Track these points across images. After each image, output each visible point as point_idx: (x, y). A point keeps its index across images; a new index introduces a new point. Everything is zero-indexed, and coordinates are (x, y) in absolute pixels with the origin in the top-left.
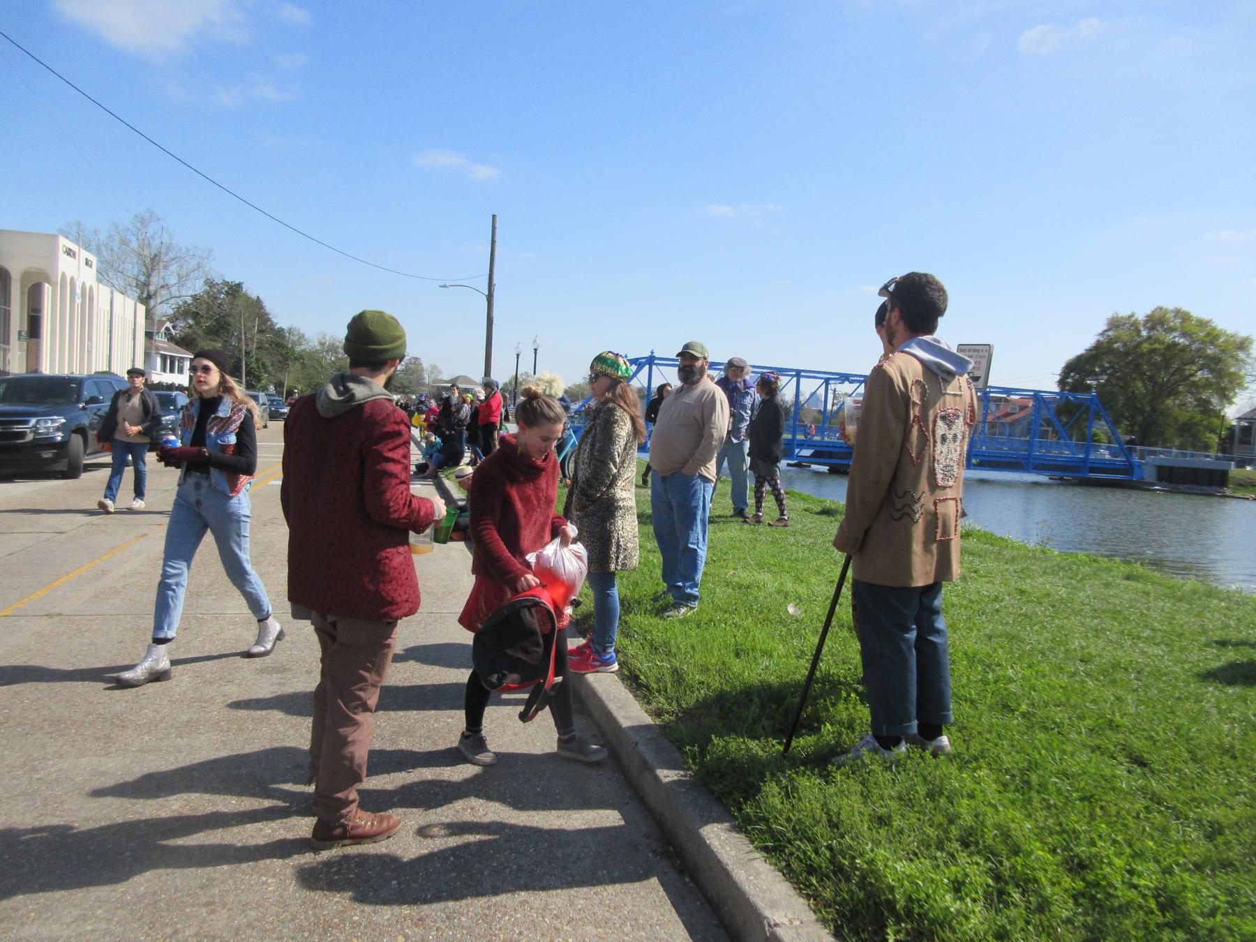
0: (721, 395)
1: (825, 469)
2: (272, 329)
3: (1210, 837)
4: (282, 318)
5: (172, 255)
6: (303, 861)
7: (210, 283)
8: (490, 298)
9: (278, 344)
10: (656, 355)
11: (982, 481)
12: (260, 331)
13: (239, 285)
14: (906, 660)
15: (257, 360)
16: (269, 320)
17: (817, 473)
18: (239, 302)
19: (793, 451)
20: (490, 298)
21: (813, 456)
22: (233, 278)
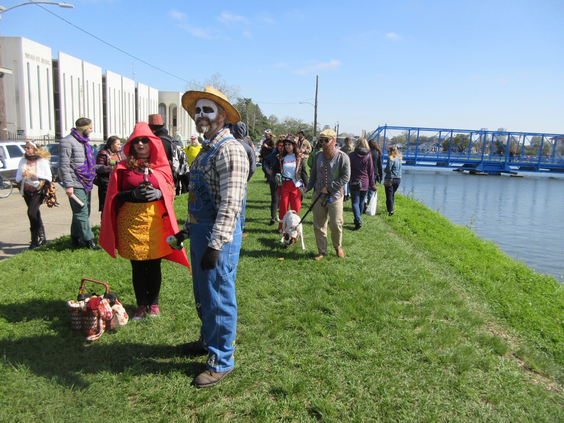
0: (36, 142)
1: (468, 172)
2: (262, 116)
3: (364, 290)
4: (266, 112)
5: (225, 90)
6: (162, 361)
7: (240, 100)
8: (316, 107)
9: (264, 123)
10: (388, 125)
11: (551, 178)
12: (256, 118)
13: (250, 100)
14: (339, 235)
15: (255, 130)
16: (261, 113)
17: (466, 174)
18: (249, 107)
19: (448, 164)
20: (316, 107)
21: (463, 166)
22: (248, 97)
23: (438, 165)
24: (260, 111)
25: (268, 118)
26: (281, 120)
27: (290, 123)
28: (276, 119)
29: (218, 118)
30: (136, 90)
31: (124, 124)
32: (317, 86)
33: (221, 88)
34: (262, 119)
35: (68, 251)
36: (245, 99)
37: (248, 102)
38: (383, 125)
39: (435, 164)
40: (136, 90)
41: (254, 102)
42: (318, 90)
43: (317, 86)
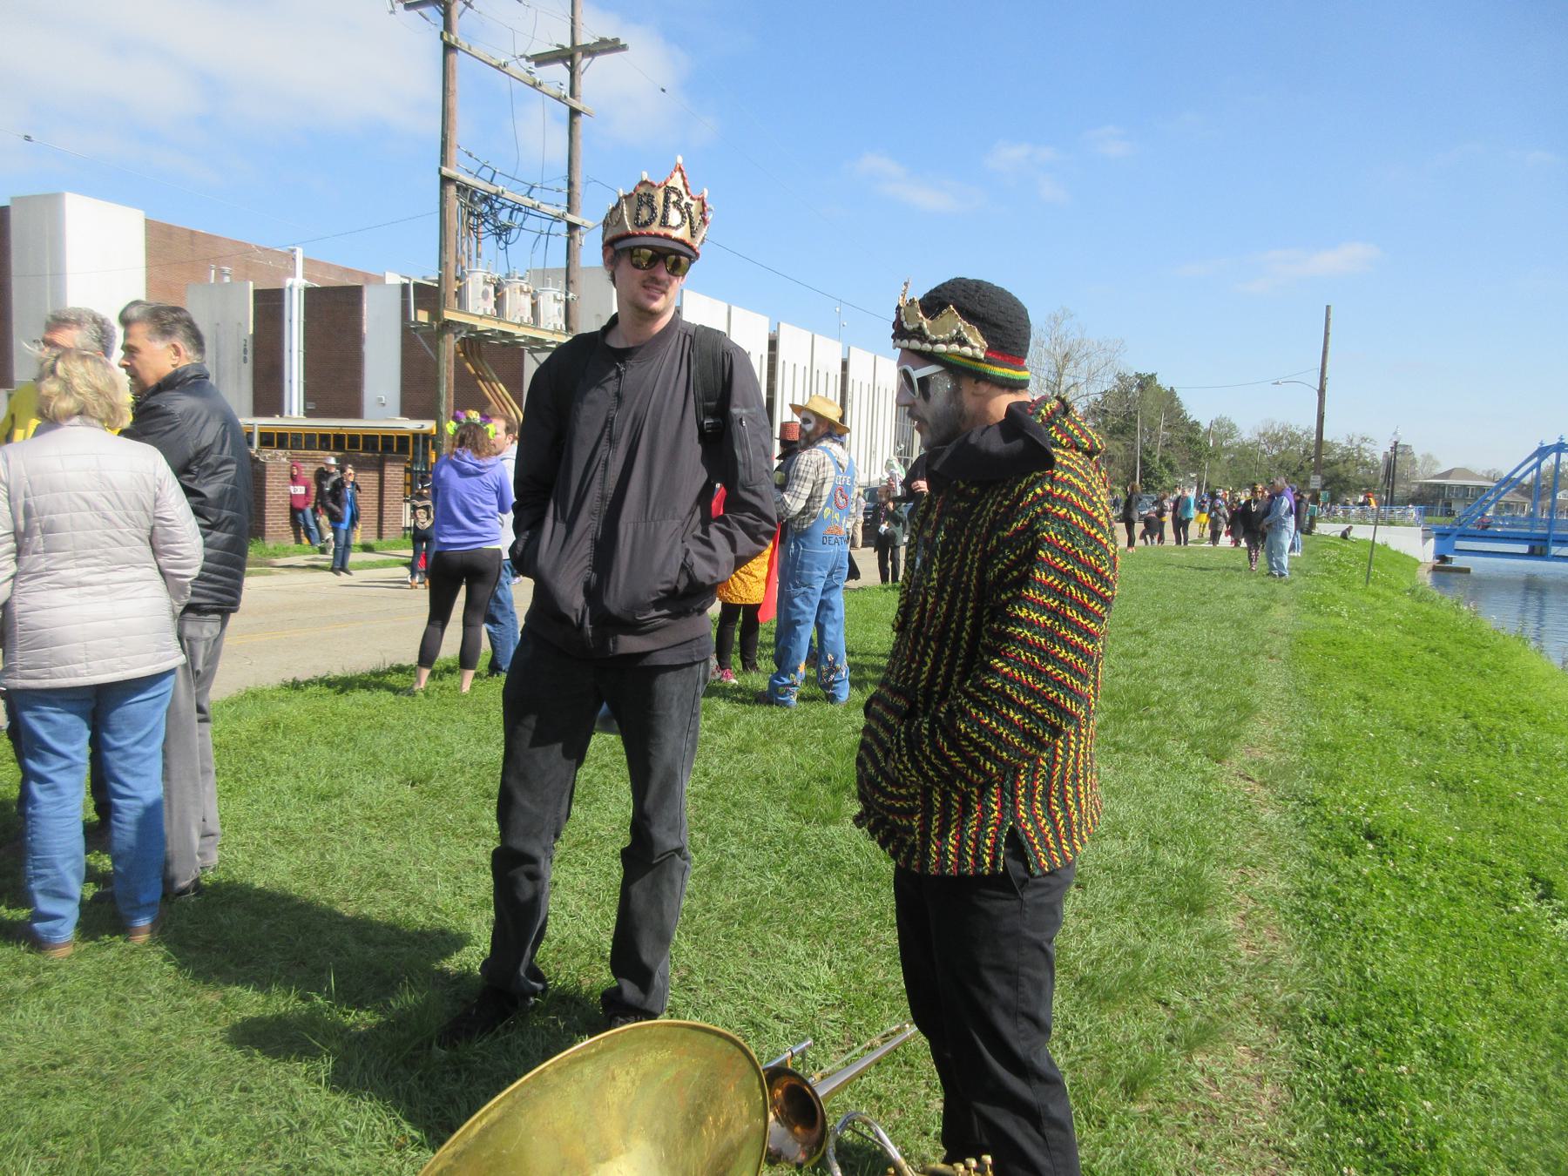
4: (1200, 409)
5: (1083, 352)
7: (1121, 378)
8: (1322, 392)
9: (1190, 440)
13: (1153, 377)
15: (1162, 459)
18: (1149, 396)
20: (1322, 392)
22: (1146, 370)
23: (1532, 554)
24: (1180, 406)
25: (1205, 425)
26: (1248, 429)
27: (1275, 440)
28: (1232, 427)
29: (816, 428)
30: (845, 365)
31: (873, 453)
32: (1327, 334)
33: (1071, 347)
34: (1184, 428)
35: (493, 844)
36: (1138, 376)
37: (1146, 382)
38: (1551, 441)
39: (1524, 548)
40: (845, 365)
41: (1164, 382)
42: (1330, 345)
43: (1327, 334)
